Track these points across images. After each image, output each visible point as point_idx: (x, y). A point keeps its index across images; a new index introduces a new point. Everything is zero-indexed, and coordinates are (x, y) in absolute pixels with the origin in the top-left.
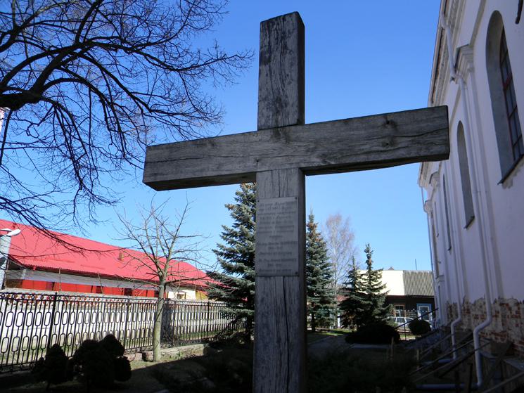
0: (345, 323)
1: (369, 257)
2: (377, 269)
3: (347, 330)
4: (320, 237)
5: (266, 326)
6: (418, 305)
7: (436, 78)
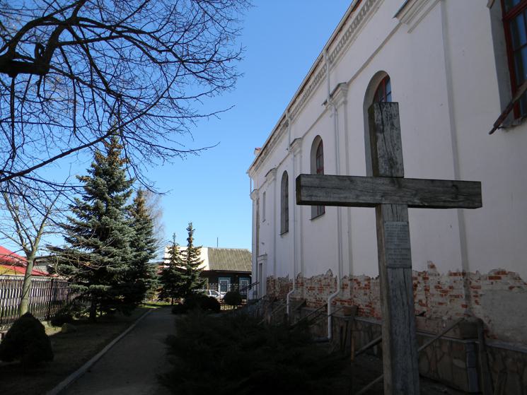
0: (161, 297)
1: (190, 235)
2: (197, 246)
3: (163, 303)
4: (147, 214)
5: (396, 296)
6: (229, 278)
7: (299, 94)
